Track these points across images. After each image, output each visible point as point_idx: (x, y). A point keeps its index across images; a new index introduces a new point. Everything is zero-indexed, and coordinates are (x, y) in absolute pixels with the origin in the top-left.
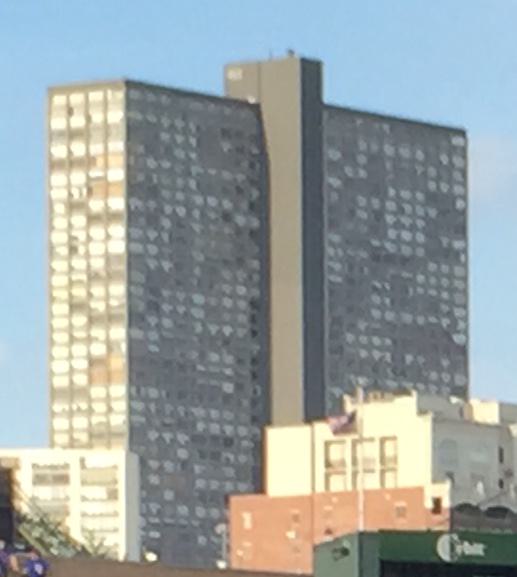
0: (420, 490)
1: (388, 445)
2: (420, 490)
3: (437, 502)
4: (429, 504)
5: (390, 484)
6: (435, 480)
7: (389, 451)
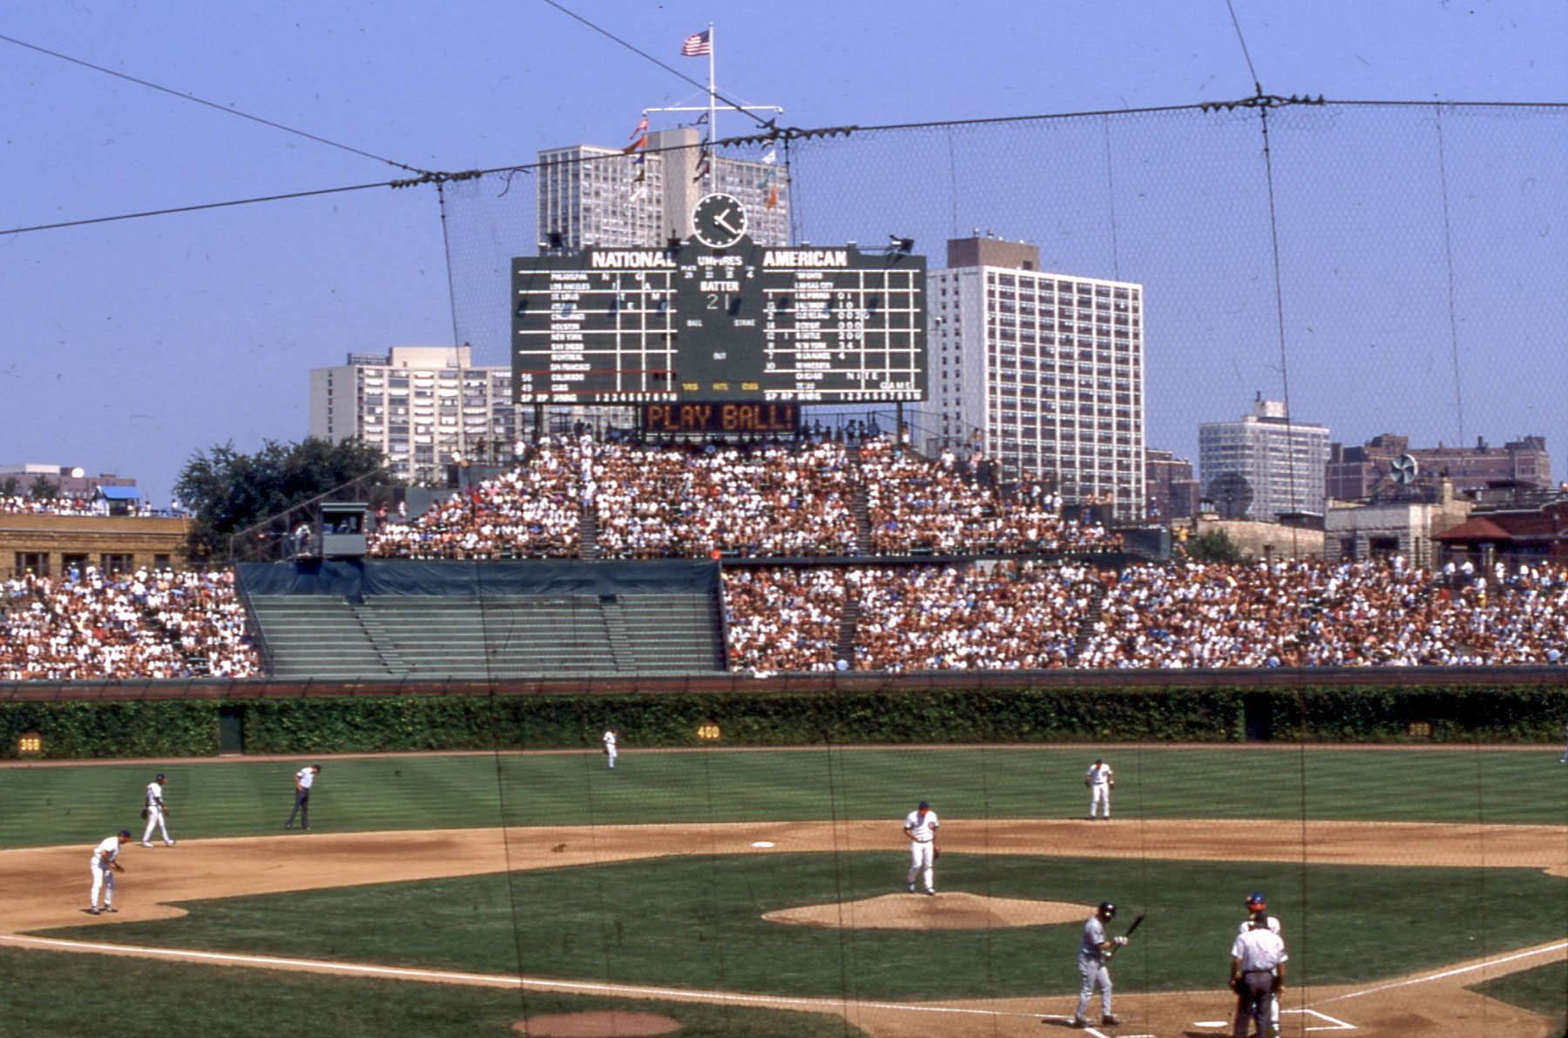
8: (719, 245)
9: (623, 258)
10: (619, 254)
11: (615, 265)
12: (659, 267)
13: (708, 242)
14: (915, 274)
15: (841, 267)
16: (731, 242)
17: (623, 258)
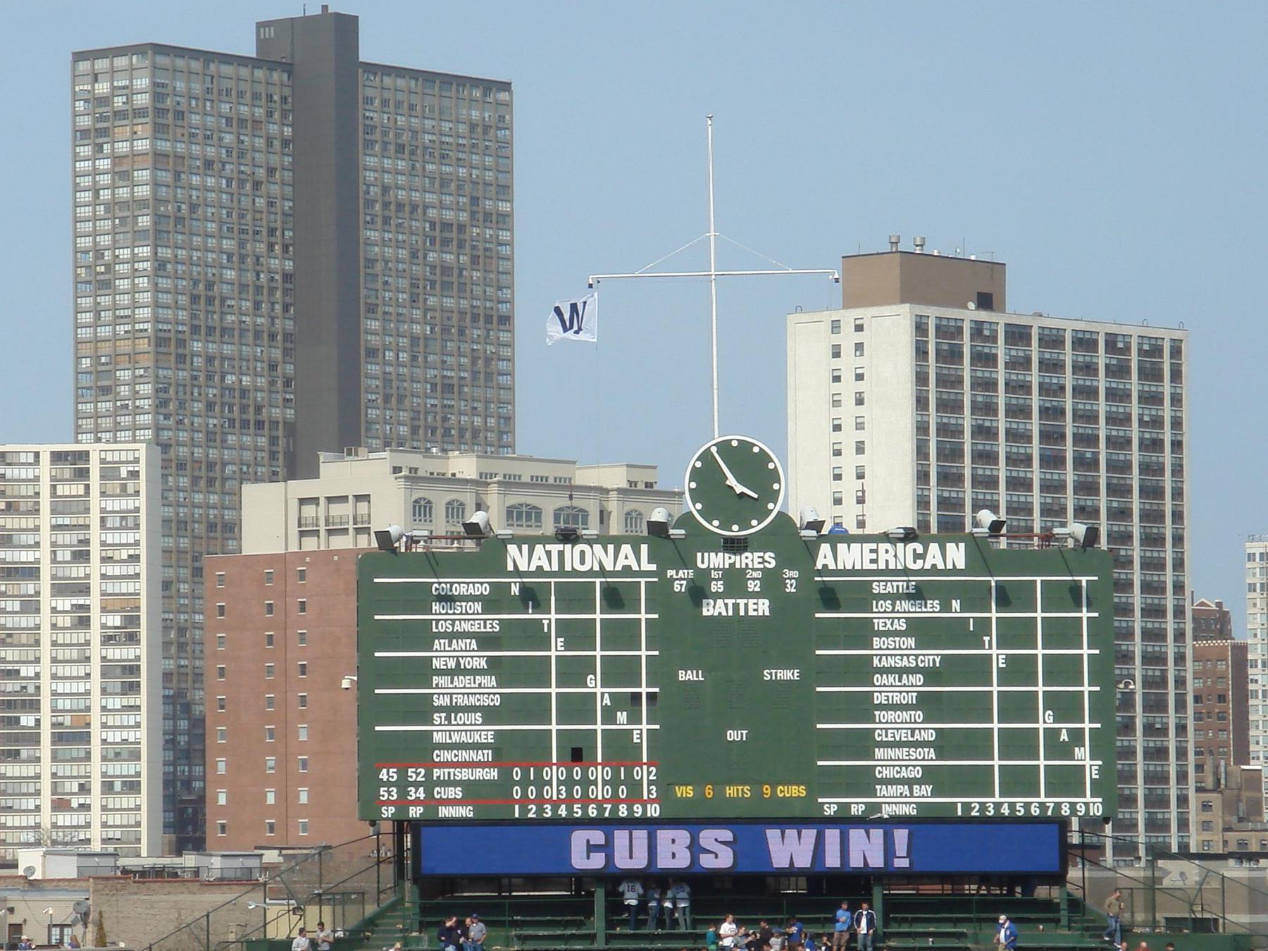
8: (735, 531)
9: (561, 554)
11: (547, 568)
12: (627, 570)
13: (714, 526)
15: (955, 571)
16: (756, 526)
17: (561, 554)
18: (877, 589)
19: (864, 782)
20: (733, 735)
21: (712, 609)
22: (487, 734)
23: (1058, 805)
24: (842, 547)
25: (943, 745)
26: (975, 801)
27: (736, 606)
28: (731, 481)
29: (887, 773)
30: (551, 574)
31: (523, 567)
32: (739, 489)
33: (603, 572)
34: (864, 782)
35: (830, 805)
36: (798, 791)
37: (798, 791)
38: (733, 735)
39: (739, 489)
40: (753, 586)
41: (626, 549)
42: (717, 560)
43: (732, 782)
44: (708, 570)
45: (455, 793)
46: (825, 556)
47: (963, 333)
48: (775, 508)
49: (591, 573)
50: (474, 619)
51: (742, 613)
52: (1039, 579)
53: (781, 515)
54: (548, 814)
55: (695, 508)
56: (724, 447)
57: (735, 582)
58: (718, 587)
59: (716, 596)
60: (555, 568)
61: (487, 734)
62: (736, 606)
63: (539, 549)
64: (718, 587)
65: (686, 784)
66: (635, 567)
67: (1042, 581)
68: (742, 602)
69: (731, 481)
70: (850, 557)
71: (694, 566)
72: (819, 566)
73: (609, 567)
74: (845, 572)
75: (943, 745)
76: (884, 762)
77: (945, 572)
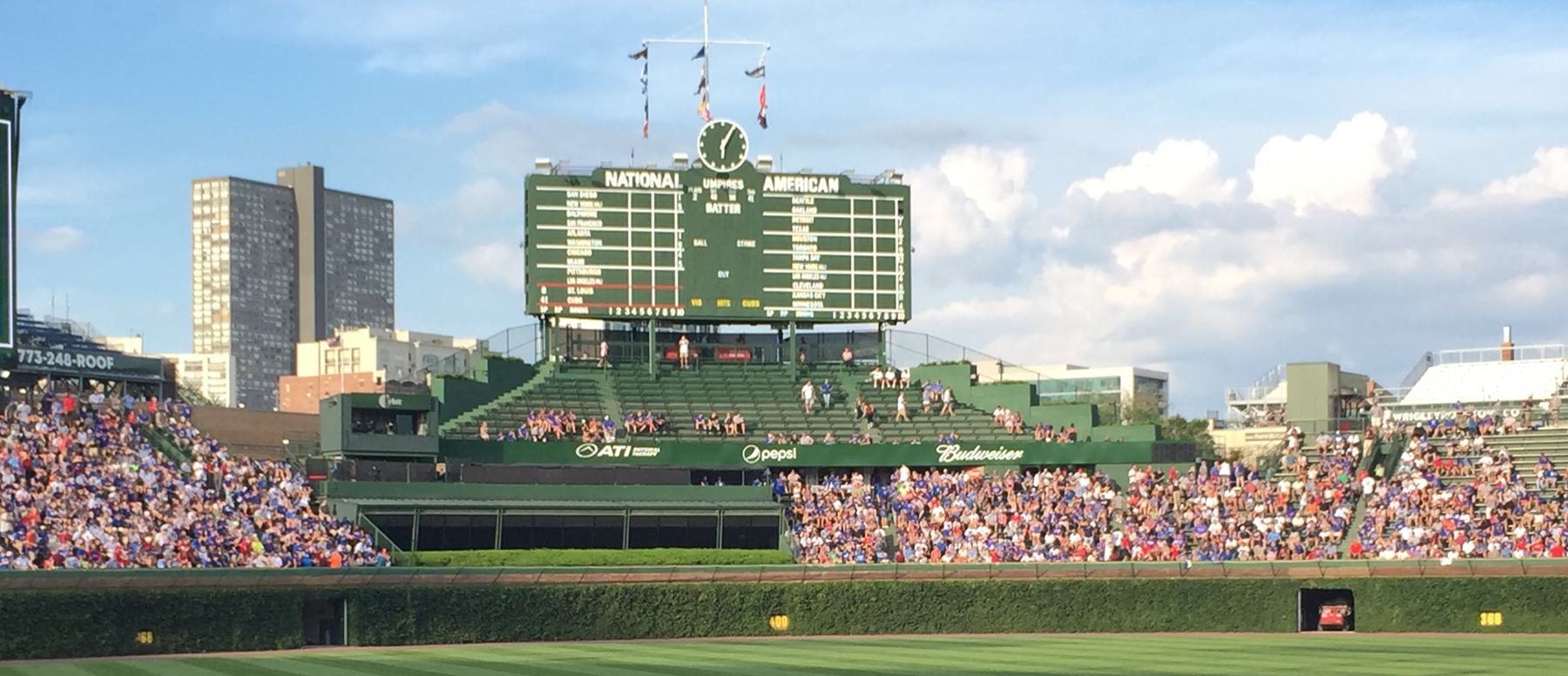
0: (371, 374)
1: (356, 352)
2: (371, 374)
3: (379, 379)
4: (375, 381)
5: (356, 371)
6: (378, 369)
7: (356, 355)
8: (723, 169)
9: (634, 178)
10: (631, 175)
11: (626, 185)
12: (668, 188)
13: (712, 166)
14: (899, 202)
15: (833, 193)
16: (734, 167)
17: (634, 178)
18: (795, 201)
19: (787, 300)
20: (721, 274)
21: (710, 208)
22: (814, 237)
23: (883, 314)
24: (777, 178)
25: (830, 282)
26: (842, 310)
27: (723, 208)
28: (724, 142)
29: (799, 296)
30: (629, 188)
31: (614, 184)
32: (722, 147)
33: (655, 188)
34: (787, 300)
35: (770, 311)
36: (755, 303)
37: (755, 303)
38: (721, 274)
39: (722, 147)
40: (733, 197)
41: (667, 176)
42: (713, 184)
43: (722, 298)
44: (709, 189)
45: (579, 300)
46: (768, 184)
47: (1420, 626)
48: (743, 158)
49: (649, 188)
50: (593, 209)
51: (726, 212)
52: (852, 198)
53: (746, 162)
54: (627, 313)
55: (703, 157)
56: (737, 132)
57: (723, 194)
58: (714, 197)
59: (713, 202)
60: (631, 185)
61: (814, 237)
62: (723, 208)
63: (622, 174)
64: (714, 197)
65: (698, 298)
66: (672, 186)
67: (855, 201)
68: (726, 205)
69: (724, 142)
70: (782, 184)
71: (702, 186)
72: (765, 189)
73: (659, 186)
74: (778, 192)
75: (830, 282)
76: (798, 290)
77: (774, 192)
